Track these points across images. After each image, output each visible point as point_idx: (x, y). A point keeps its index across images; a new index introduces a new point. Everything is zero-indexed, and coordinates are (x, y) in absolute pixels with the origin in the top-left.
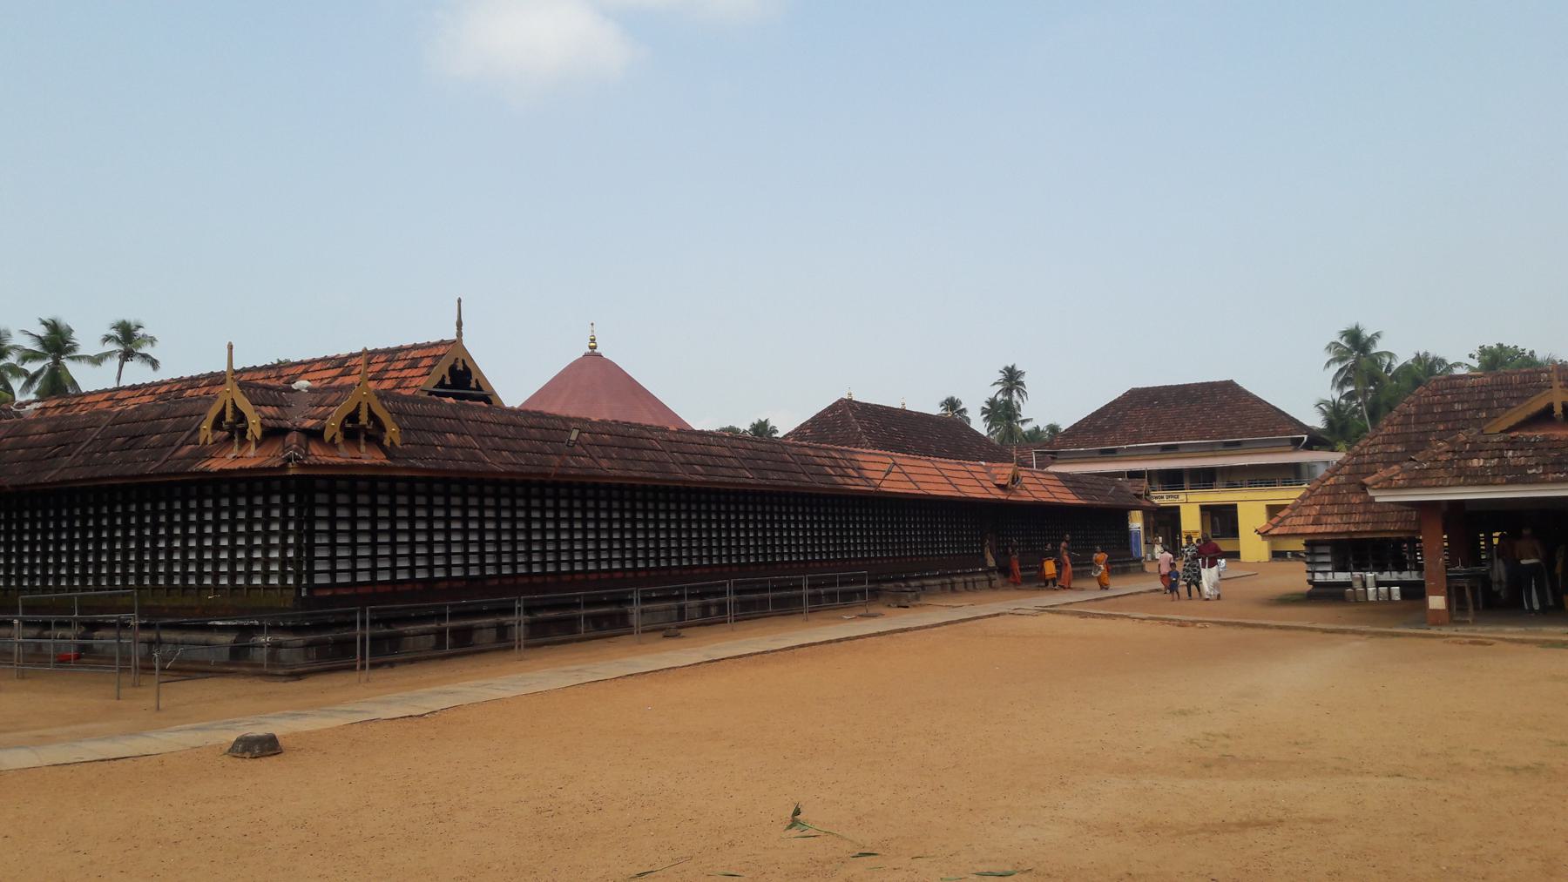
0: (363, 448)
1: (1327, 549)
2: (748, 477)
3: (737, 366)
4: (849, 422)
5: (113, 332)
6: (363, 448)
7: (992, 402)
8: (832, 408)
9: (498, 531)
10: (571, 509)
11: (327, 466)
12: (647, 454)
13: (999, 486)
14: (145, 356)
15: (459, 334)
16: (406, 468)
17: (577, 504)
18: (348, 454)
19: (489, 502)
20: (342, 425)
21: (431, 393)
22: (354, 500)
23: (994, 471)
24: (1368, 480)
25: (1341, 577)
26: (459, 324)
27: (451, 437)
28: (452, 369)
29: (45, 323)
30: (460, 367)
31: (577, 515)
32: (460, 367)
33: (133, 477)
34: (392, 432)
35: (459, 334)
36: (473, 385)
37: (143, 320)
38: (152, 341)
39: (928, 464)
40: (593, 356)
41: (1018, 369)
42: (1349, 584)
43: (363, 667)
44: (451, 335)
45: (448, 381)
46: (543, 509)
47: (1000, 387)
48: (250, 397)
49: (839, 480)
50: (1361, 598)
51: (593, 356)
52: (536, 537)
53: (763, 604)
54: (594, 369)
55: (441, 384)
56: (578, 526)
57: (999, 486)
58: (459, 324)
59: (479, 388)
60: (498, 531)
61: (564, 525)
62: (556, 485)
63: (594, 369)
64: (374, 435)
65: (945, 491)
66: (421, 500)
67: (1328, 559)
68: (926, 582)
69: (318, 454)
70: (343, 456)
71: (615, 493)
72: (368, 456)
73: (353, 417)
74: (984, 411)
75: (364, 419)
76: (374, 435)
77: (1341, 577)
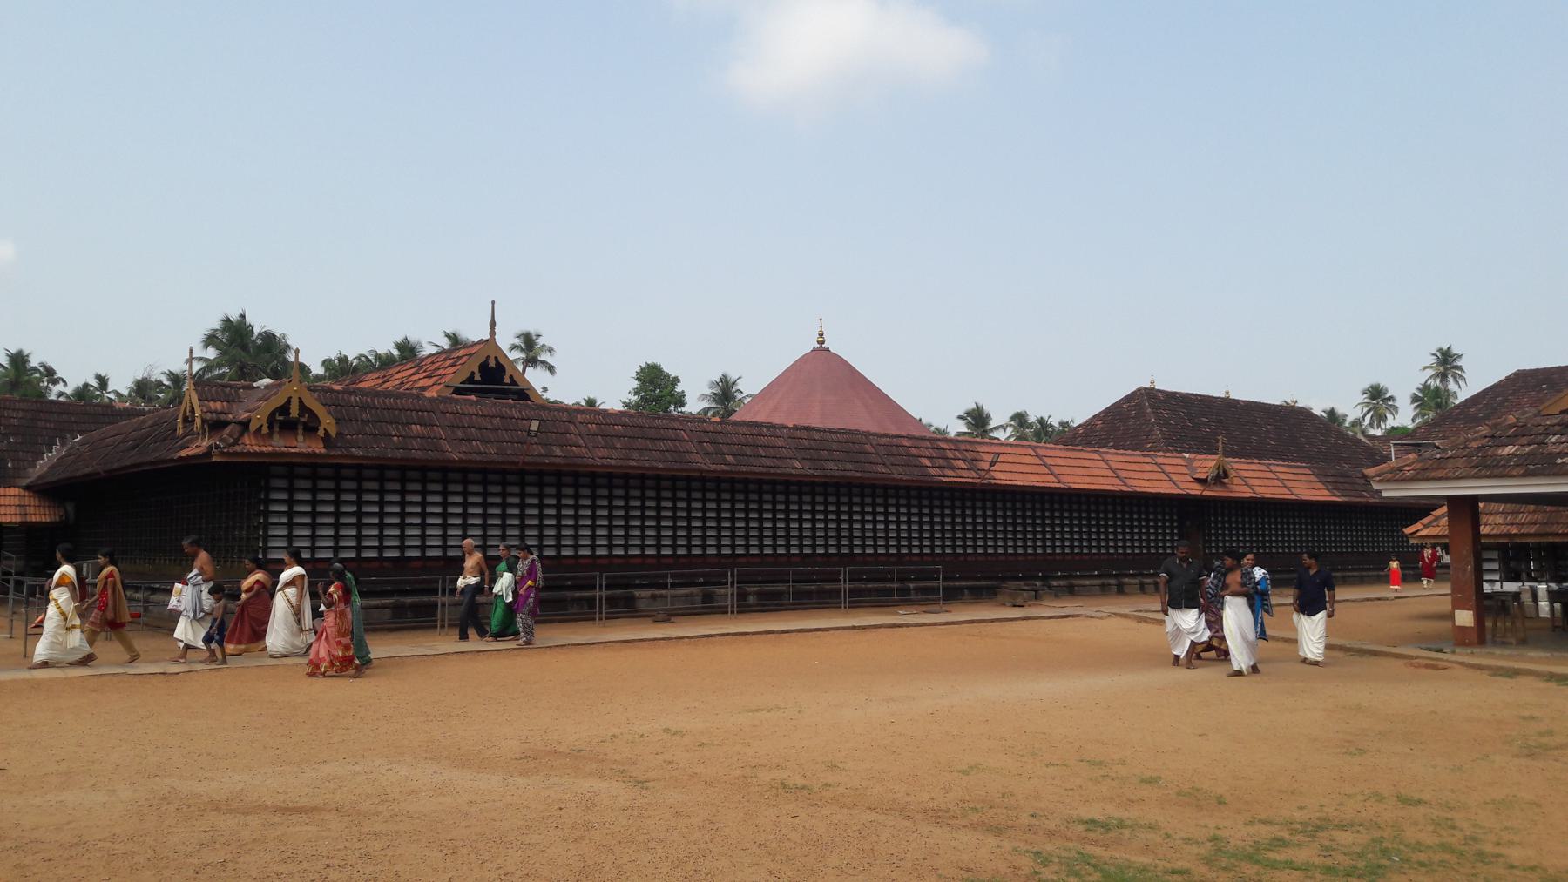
0: (300, 438)
1: (1495, 555)
2: (798, 466)
3: (994, 352)
4: (1148, 417)
5: (517, 341)
6: (300, 438)
7: (1425, 388)
8: (1128, 398)
9: (826, 521)
10: (953, 508)
11: (262, 454)
12: (662, 445)
13: (1199, 481)
14: (543, 363)
15: (493, 333)
16: (341, 456)
17: (958, 503)
18: (282, 443)
19: (925, 502)
20: (273, 414)
21: (458, 391)
22: (658, 494)
23: (1196, 464)
24: (1370, 472)
25: (1511, 587)
26: (493, 324)
27: (416, 429)
28: (484, 367)
29: (447, 336)
30: (492, 364)
31: (844, 508)
32: (492, 364)
33: (151, 463)
34: (327, 422)
35: (493, 333)
36: (507, 380)
37: (541, 330)
38: (550, 350)
39: (1096, 456)
40: (821, 351)
41: (1455, 351)
42: (1516, 596)
43: (443, 626)
44: (487, 337)
45: (478, 377)
46: (942, 507)
47: (1431, 372)
48: (319, 399)
49: (932, 471)
50: (1531, 613)
51: (821, 351)
52: (959, 535)
53: (935, 590)
54: (823, 368)
55: (471, 379)
56: (969, 520)
57: (1199, 481)
58: (493, 324)
59: (513, 382)
60: (826, 529)
61: (958, 520)
62: (837, 485)
63: (823, 368)
64: (311, 428)
65: (1050, 482)
66: (794, 498)
67: (1495, 566)
68: (1075, 582)
69: (250, 444)
70: (279, 444)
71: (978, 495)
72: (301, 445)
73: (284, 409)
74: (1415, 399)
75: (294, 411)
76: (311, 428)
77: (1511, 587)
